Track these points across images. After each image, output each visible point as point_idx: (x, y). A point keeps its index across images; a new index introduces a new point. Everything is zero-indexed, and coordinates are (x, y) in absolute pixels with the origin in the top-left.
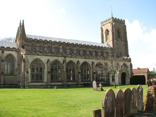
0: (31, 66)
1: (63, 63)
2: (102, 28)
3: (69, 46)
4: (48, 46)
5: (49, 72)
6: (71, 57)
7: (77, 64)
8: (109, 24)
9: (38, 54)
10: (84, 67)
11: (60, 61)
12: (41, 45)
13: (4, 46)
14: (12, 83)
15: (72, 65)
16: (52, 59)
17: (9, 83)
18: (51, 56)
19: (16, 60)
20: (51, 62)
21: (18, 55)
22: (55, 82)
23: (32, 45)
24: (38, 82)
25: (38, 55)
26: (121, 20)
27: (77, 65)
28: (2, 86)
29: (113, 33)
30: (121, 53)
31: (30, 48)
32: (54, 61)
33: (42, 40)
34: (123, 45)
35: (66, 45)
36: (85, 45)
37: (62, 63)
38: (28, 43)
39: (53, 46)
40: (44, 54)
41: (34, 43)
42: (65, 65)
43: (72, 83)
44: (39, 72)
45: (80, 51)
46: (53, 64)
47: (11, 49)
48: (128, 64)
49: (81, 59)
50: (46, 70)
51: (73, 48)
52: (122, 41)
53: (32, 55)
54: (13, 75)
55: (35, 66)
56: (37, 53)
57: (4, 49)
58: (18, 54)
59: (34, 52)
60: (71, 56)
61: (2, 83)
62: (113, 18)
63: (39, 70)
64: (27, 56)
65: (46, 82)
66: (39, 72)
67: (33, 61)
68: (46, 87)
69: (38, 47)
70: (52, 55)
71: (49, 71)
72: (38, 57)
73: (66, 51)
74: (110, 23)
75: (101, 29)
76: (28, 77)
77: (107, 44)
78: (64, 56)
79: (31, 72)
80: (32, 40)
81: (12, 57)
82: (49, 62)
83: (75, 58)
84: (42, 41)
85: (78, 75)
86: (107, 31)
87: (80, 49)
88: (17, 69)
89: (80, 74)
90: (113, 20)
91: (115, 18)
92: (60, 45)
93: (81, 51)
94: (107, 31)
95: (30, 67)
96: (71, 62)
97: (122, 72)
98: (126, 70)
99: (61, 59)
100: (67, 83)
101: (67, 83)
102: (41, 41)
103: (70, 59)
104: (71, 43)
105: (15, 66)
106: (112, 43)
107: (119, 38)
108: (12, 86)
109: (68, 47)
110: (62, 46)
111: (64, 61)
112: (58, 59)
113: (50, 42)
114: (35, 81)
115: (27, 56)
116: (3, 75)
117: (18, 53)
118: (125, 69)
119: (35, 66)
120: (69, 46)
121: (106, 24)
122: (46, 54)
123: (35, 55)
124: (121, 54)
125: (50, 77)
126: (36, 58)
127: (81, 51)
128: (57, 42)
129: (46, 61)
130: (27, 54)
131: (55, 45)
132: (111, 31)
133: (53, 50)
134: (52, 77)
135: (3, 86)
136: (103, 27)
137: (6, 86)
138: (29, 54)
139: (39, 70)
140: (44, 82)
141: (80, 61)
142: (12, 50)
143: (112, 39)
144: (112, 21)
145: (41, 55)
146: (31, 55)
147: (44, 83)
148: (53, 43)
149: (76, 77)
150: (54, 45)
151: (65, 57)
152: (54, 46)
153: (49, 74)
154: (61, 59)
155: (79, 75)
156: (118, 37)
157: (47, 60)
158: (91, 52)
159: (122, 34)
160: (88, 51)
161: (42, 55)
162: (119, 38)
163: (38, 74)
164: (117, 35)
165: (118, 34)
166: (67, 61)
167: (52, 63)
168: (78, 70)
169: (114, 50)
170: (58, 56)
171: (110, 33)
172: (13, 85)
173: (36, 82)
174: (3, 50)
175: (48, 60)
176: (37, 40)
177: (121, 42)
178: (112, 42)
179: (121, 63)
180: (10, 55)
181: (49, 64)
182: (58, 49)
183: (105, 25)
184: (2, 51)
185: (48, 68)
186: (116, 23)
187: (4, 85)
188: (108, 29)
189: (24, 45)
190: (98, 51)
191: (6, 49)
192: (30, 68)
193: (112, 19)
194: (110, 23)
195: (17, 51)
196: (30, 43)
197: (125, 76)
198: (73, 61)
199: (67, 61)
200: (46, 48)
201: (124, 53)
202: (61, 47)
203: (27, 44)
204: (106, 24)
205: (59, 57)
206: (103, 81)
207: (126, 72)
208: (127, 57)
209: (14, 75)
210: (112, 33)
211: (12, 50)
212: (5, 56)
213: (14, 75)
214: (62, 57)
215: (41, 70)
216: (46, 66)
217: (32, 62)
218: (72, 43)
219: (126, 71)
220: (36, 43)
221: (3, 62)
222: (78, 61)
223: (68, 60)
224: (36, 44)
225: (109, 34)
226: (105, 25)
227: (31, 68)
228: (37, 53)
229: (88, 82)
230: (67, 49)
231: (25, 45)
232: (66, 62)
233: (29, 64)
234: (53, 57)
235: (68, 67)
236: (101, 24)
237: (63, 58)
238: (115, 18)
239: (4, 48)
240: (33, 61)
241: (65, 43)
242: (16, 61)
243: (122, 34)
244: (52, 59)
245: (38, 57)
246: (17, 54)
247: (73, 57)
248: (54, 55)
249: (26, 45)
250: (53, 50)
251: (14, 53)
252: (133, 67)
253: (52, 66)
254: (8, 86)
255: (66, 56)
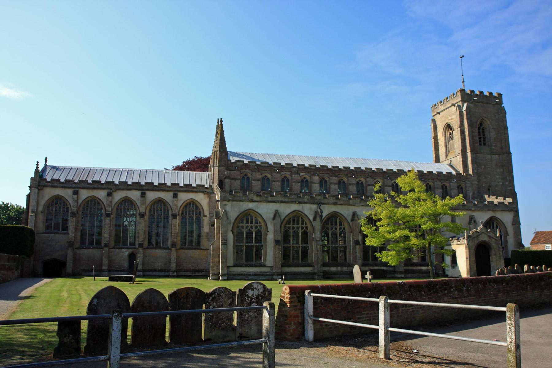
0: (236, 226)
1: (315, 219)
2: (434, 121)
3: (337, 176)
4: (283, 176)
5: (277, 242)
6: (335, 204)
7: (352, 220)
8: (454, 109)
9: (250, 197)
10: (332, 228)
11: (306, 213)
12: (265, 174)
13: (203, 184)
14: (197, 268)
15: (338, 224)
16: (286, 209)
17: (190, 267)
18: (282, 202)
19: (207, 213)
20: (283, 217)
21: (210, 201)
22: (292, 267)
23: (243, 177)
24: (251, 266)
25: (252, 201)
26: (491, 94)
27: (351, 223)
28: (173, 274)
29: (462, 133)
30: (490, 186)
31: (239, 184)
32: (291, 215)
33: (280, 164)
34: (496, 165)
35: (329, 174)
36: (381, 171)
37: (311, 218)
38: (232, 172)
39: (294, 176)
40: (267, 198)
41: (247, 171)
42: (317, 224)
43: (339, 268)
44: (244, 241)
45: (366, 187)
46: (289, 222)
47: (194, 187)
48: (506, 218)
49: (362, 207)
50: (270, 237)
51: (348, 179)
52: (492, 153)
53: (236, 201)
54: (198, 249)
55: (245, 228)
56: (248, 196)
57: (178, 189)
58: (209, 200)
59: (228, 194)
60: (335, 201)
61: (173, 266)
62: (462, 91)
63: (245, 236)
64: (225, 205)
65: (270, 265)
66: (244, 241)
67: (240, 216)
68: (271, 277)
69: (259, 180)
70: (287, 200)
71: (279, 238)
72: (251, 205)
73: (330, 188)
74: (454, 105)
75: (432, 125)
76: (227, 254)
77: (450, 165)
78: (316, 201)
79: (234, 243)
80: (243, 165)
81: (197, 206)
82: (277, 217)
83: (346, 207)
84: (266, 165)
85: (354, 248)
86: (448, 127)
87: (366, 181)
88: (208, 233)
89: (358, 247)
90: (462, 98)
91: (469, 92)
92: (314, 175)
93: (369, 185)
94: (448, 127)
95: (231, 231)
96: (334, 216)
97: (476, 242)
98: (492, 235)
99: (308, 210)
100: (326, 269)
101: (326, 269)
102: (265, 166)
103: (333, 209)
104: (341, 167)
105: (203, 227)
106: (461, 159)
107: (485, 144)
108: (197, 274)
109: (334, 178)
110: (318, 175)
111: (316, 213)
112: (301, 210)
113: (289, 167)
114: (244, 261)
115: (225, 205)
116: (143, 247)
117: (209, 197)
118: (488, 232)
119: (245, 228)
120: (337, 174)
121: (444, 110)
122: (270, 199)
123: (243, 201)
124: (489, 190)
125: (280, 254)
126: (247, 208)
127: (369, 185)
128: (307, 165)
129: (272, 216)
130: (226, 201)
131: (301, 174)
132: (456, 127)
133: (296, 187)
134: (286, 256)
135: (175, 274)
136: (437, 118)
137: (183, 273)
138: (229, 201)
139: (245, 236)
140: (264, 266)
141: (359, 213)
142: (195, 190)
143: (462, 150)
144: (460, 99)
145: (258, 202)
146: (235, 202)
147: (265, 268)
148: (295, 169)
149: (350, 254)
150: (298, 174)
151: (319, 204)
152: (298, 176)
153: (277, 247)
154: (308, 210)
155: (356, 247)
156: (480, 144)
157: (274, 212)
158: (364, 186)
159: (491, 135)
160: (389, 186)
161: (261, 202)
162: (485, 144)
163: (299, 246)
164: (478, 139)
165: (479, 134)
166: (324, 215)
167: (287, 219)
168: (353, 235)
169: (467, 178)
170: (300, 203)
171: (457, 134)
172: (198, 271)
173: (246, 266)
174: (176, 191)
175: (276, 213)
176: (254, 164)
177: (488, 157)
178: (462, 158)
179: (482, 217)
180: (160, 201)
181: (278, 221)
182: (305, 183)
183: (442, 111)
184: (142, 193)
185: (275, 232)
186: (472, 105)
187: (143, 271)
188: (449, 122)
189: (223, 178)
190: (450, 186)
191: (182, 189)
192: (233, 233)
193: (459, 94)
194: (453, 105)
195: (208, 192)
196: (238, 173)
197: (489, 253)
198: (342, 213)
199: (324, 215)
200: (278, 181)
201: (501, 185)
202: (316, 178)
203: (230, 173)
204: (444, 110)
205: (304, 205)
206: (309, 265)
207: (491, 242)
208: (504, 199)
209: (201, 249)
210: (459, 132)
211: (195, 190)
212: (180, 204)
213: (201, 249)
214: (312, 203)
215: (260, 237)
216: (271, 227)
217: (238, 217)
218: (344, 167)
219: (489, 237)
220: (253, 171)
221: (175, 220)
222: (354, 214)
223: (327, 210)
224: (254, 173)
225: (455, 138)
226: (442, 111)
227: (236, 233)
228: (248, 196)
229: (383, 268)
230: (331, 183)
231: (225, 179)
232: (321, 216)
233: (230, 223)
234: (289, 204)
235: (328, 229)
236: (433, 111)
237: (314, 207)
238: (469, 92)
239: (177, 186)
240: (240, 216)
241: (325, 168)
242: (206, 216)
243: (492, 134)
244: (286, 209)
245: (251, 205)
246: (208, 199)
247: (342, 202)
248: (290, 200)
249: (229, 178)
250: (296, 187)
251: (201, 199)
252: (521, 226)
253: (285, 227)
254: (188, 273)
255: (322, 202)
